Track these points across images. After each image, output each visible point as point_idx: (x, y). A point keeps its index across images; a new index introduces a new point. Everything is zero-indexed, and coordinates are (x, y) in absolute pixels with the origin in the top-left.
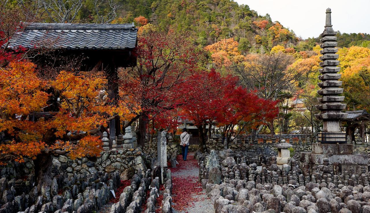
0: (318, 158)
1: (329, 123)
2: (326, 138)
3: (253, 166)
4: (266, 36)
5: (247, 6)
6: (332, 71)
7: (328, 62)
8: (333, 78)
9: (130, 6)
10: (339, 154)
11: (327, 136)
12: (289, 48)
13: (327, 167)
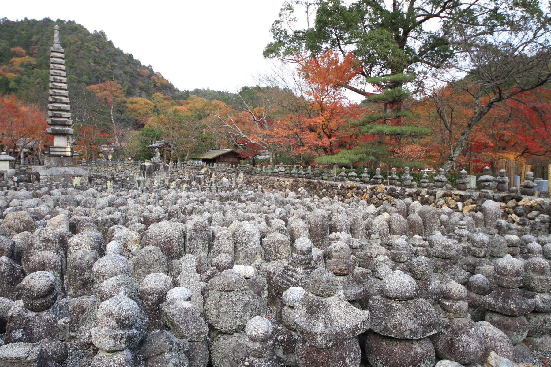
4: (148, 83)
5: (131, 55)
7: (54, 79)
9: (7, 35)
10: (62, 166)
12: (167, 96)
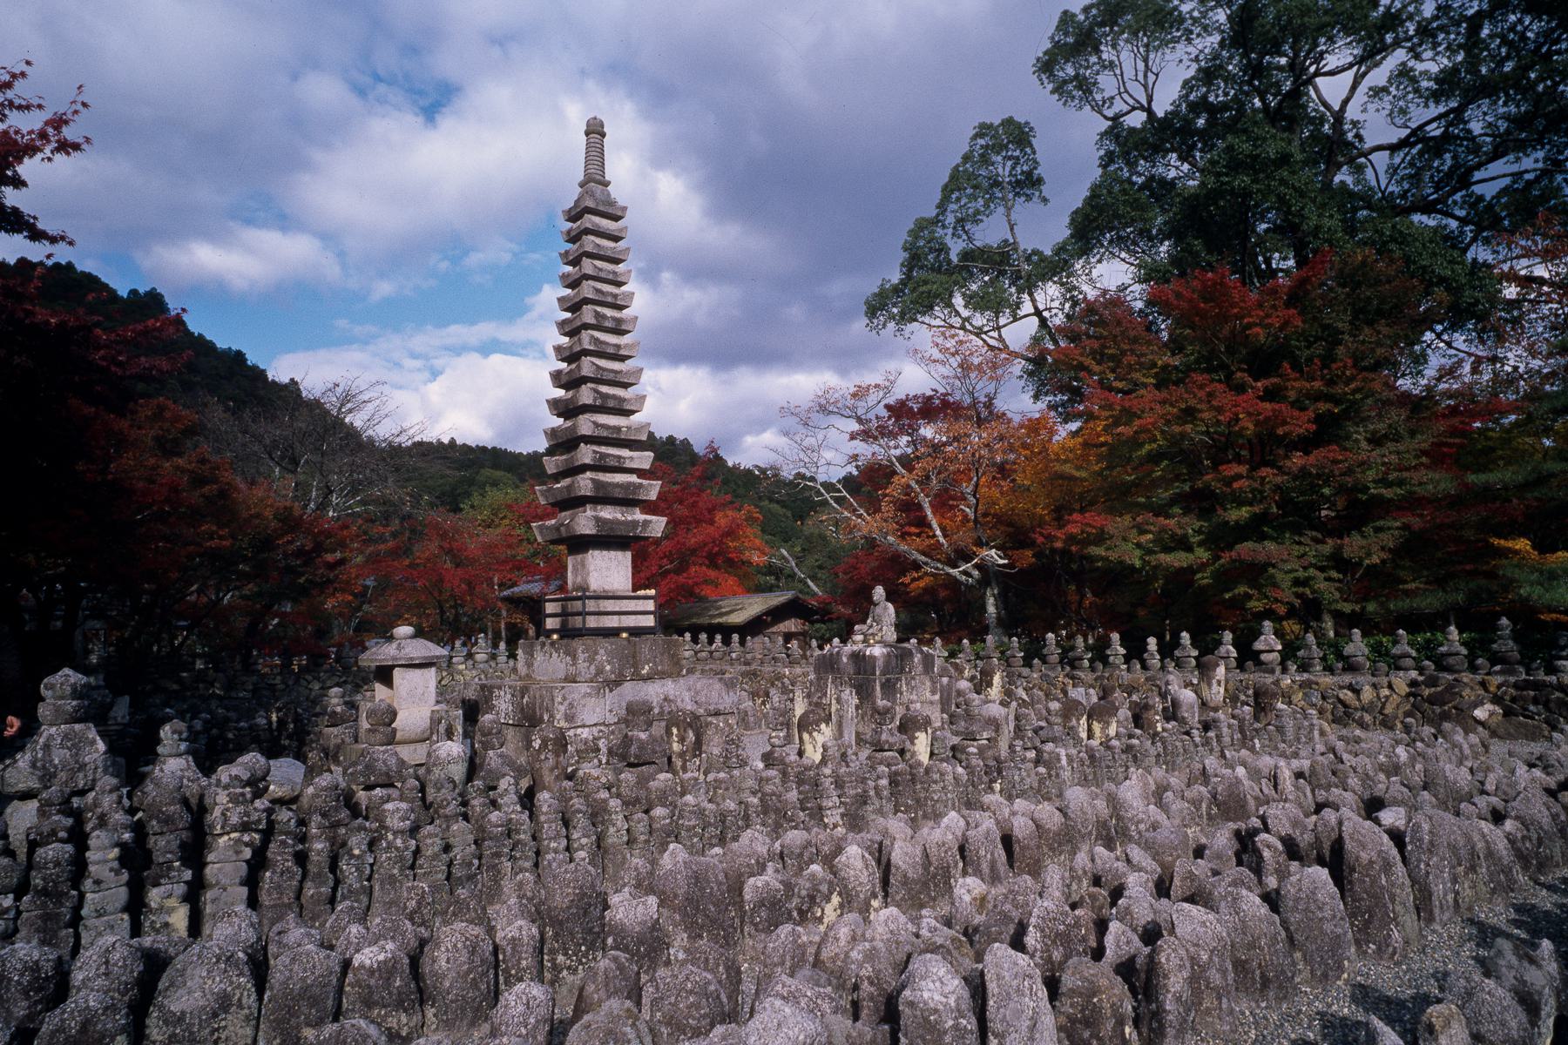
0: (564, 699)
1: (596, 553)
2: (584, 614)
3: (245, 776)
6: (611, 350)
8: (611, 376)
11: (591, 605)
13: (643, 736)
